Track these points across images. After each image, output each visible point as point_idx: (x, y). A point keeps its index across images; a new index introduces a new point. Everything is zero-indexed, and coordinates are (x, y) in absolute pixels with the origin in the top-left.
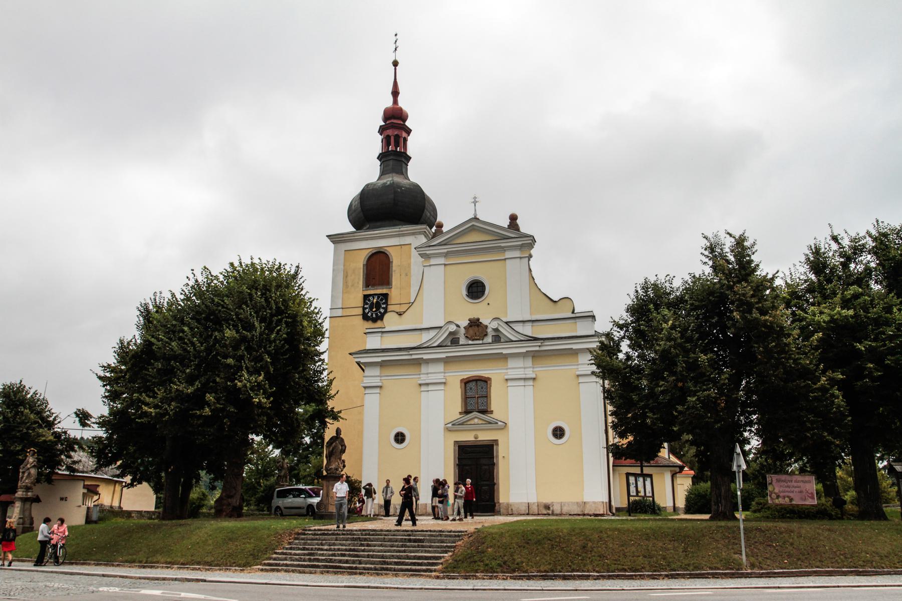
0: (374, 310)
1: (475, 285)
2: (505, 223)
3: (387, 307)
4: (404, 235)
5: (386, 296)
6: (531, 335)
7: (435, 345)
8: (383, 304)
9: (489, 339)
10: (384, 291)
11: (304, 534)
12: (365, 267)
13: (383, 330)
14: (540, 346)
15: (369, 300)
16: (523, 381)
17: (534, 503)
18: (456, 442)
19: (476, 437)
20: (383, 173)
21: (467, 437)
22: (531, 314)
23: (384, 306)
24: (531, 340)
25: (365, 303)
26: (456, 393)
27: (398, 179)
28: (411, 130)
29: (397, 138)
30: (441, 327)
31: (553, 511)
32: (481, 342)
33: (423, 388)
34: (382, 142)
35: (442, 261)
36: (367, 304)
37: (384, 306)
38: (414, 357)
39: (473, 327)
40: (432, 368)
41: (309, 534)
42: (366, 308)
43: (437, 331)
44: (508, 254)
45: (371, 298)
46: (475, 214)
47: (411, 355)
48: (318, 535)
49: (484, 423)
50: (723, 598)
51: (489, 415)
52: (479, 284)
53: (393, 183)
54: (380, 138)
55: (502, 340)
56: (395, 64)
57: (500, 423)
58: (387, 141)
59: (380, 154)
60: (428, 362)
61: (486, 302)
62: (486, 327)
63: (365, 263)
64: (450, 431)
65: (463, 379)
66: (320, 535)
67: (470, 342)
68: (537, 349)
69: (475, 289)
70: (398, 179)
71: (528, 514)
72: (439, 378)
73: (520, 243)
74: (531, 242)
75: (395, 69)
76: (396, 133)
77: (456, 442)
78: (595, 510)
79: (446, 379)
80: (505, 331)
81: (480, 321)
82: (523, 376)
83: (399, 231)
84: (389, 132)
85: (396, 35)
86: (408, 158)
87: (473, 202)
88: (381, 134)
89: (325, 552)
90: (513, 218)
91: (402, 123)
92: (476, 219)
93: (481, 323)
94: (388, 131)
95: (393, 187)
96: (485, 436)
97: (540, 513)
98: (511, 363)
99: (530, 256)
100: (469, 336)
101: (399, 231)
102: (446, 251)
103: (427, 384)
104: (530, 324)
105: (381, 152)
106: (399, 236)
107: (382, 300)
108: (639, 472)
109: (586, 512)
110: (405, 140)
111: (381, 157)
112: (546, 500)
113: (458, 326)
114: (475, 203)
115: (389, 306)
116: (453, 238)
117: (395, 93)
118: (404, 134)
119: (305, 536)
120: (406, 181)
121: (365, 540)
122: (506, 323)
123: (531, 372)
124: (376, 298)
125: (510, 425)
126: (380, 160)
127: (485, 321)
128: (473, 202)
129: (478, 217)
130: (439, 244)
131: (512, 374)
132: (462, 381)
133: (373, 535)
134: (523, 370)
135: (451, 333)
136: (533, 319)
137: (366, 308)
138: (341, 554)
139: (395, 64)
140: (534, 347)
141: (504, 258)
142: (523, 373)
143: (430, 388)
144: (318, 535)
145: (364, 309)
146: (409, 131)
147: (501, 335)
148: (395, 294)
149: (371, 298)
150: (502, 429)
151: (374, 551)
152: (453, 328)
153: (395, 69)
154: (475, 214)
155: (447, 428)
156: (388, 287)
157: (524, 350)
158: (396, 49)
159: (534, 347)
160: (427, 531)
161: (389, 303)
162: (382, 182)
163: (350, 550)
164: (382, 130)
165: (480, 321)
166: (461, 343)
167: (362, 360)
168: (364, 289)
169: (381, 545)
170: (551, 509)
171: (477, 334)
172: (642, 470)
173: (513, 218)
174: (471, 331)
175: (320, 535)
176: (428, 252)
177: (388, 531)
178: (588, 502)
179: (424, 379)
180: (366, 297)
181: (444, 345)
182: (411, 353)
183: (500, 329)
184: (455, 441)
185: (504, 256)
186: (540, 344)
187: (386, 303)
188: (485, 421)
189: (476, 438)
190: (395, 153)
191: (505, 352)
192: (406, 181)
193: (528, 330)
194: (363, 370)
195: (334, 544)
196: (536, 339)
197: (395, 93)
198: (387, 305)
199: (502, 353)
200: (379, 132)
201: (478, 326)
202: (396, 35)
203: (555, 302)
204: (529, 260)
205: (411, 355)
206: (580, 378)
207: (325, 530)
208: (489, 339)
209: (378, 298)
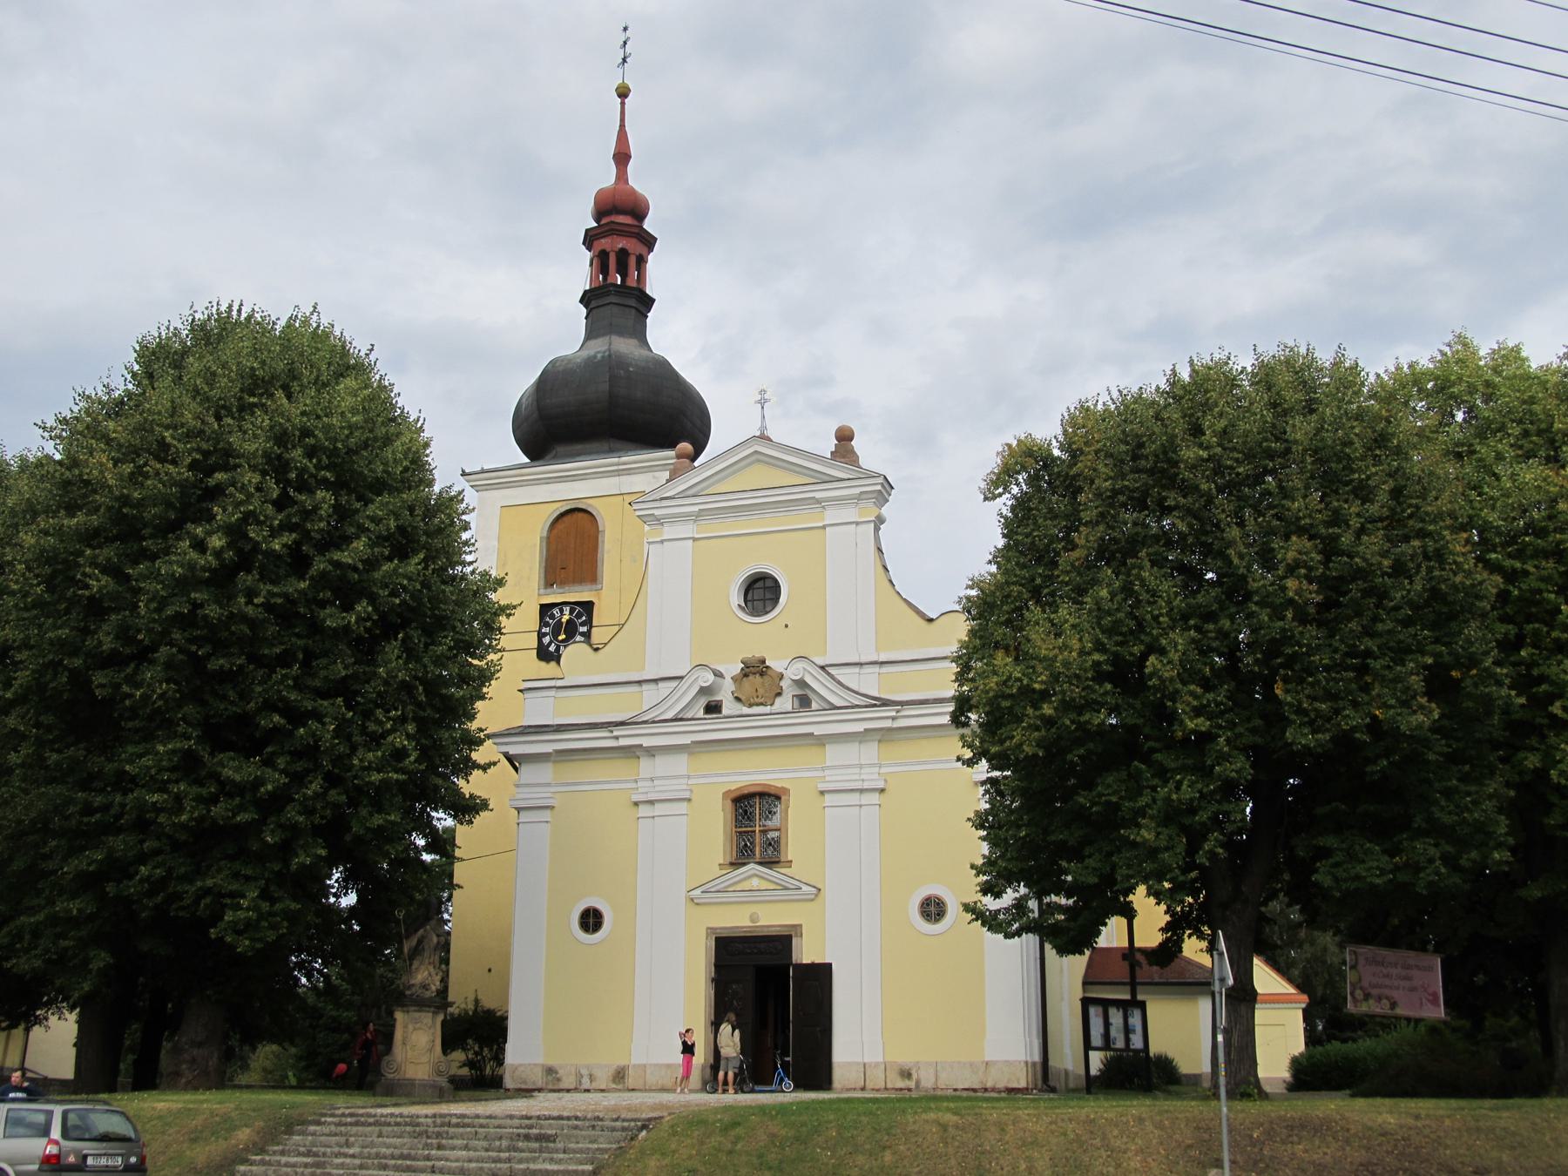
0: (562, 637)
1: (760, 584)
2: (828, 445)
3: (589, 631)
4: (629, 472)
5: (588, 607)
6: (876, 694)
7: (669, 715)
8: (583, 624)
9: (785, 703)
10: (584, 596)
11: (318, 1123)
12: (544, 544)
13: (559, 683)
14: (894, 718)
15: (553, 616)
16: (857, 795)
17: (877, 1065)
18: (710, 930)
19: (753, 918)
20: (591, 333)
21: (738, 919)
22: (877, 650)
23: (583, 629)
24: (875, 705)
25: (543, 623)
26: (717, 824)
27: (624, 346)
28: (655, 239)
29: (623, 255)
30: (681, 678)
31: (918, 1083)
32: (767, 709)
33: (644, 811)
34: (591, 265)
35: (688, 530)
36: (547, 625)
37: (583, 629)
38: (623, 742)
39: (751, 677)
40: (662, 765)
41: (329, 1124)
42: (545, 635)
43: (674, 684)
44: (831, 516)
45: (556, 612)
46: (763, 428)
47: (617, 738)
48: (346, 1124)
49: (772, 886)
50: (91, 1097)
51: (783, 870)
52: (769, 583)
53: (610, 356)
54: (588, 255)
55: (814, 706)
56: (623, 93)
57: (805, 888)
58: (601, 262)
59: (586, 292)
60: (651, 752)
61: (781, 621)
62: (781, 677)
63: (545, 534)
64: (697, 904)
65: (729, 791)
66: (351, 1124)
67: (746, 710)
68: (888, 724)
69: (758, 594)
70: (624, 346)
71: (863, 1089)
72: (676, 788)
73: (857, 491)
74: (879, 487)
75: (623, 104)
76: (620, 246)
77: (710, 930)
78: (1008, 1082)
79: (691, 791)
80: (818, 683)
81: (767, 663)
82: (858, 785)
83: (618, 464)
84: (605, 243)
85: (625, 29)
86: (648, 302)
87: (759, 402)
88: (589, 249)
89: (348, 1161)
90: (845, 437)
91: (636, 223)
92: (764, 438)
93: (767, 667)
94: (603, 241)
95: (613, 366)
96: (770, 918)
97: (889, 1086)
98: (833, 754)
99: (880, 520)
100: (743, 698)
101: (618, 464)
102: (696, 508)
103: (652, 802)
104: (876, 669)
105: (588, 288)
106: (619, 473)
107: (579, 616)
108: (1127, 997)
109: (989, 1085)
110: (641, 261)
111: (586, 299)
112: (905, 1058)
113: (718, 674)
114: (762, 403)
115: (594, 630)
116: (711, 480)
117: (622, 157)
118: (641, 249)
119: (318, 1128)
120: (645, 352)
121: (439, 1135)
122: (822, 668)
123: (876, 776)
124: (567, 610)
125: (827, 893)
126: (586, 306)
127: (775, 664)
128: (759, 402)
129: (769, 433)
130: (682, 495)
131: (834, 779)
132: (726, 794)
133: (457, 1125)
134: (857, 770)
135: (703, 691)
136: (881, 660)
137: (545, 635)
138: (380, 1164)
139: (623, 93)
140: (882, 719)
141: (821, 524)
142: (857, 777)
143: (659, 809)
144: (346, 1124)
145: (541, 636)
146: (649, 242)
147: (811, 695)
148: (607, 601)
149: (556, 612)
150: (812, 900)
151: (447, 1160)
152: (709, 678)
153: (623, 104)
154: (763, 428)
155: (692, 900)
156: (594, 587)
157: (860, 727)
158: (624, 60)
159: (882, 719)
160: (568, 1118)
161: (594, 624)
162: (585, 353)
163: (402, 1157)
164: (590, 239)
165: (767, 663)
166: (725, 711)
167: (513, 750)
168: (542, 591)
169: (466, 1148)
170: (915, 1076)
171: (761, 691)
172: (1134, 994)
173: (845, 437)
174: (748, 684)
175: (351, 1124)
176: (656, 512)
177: (490, 1117)
178: (995, 1063)
179: (644, 791)
180: (545, 609)
181: (689, 715)
182: (615, 733)
183: (808, 680)
184: (708, 928)
185: (823, 520)
186: (894, 714)
187: (589, 622)
188: (777, 884)
189: (752, 921)
190: (623, 290)
191: (818, 730)
192: (645, 352)
193: (869, 683)
194: (516, 769)
195: (372, 1145)
196: (885, 703)
197: (622, 157)
198: (591, 627)
199: (641, 746)
200: (584, 243)
201: (762, 674)
202: (625, 29)
203: (931, 620)
204: (877, 529)
205: (617, 738)
206: (827, 796)
207: (362, 1115)
208: (785, 703)
209: (571, 613)
